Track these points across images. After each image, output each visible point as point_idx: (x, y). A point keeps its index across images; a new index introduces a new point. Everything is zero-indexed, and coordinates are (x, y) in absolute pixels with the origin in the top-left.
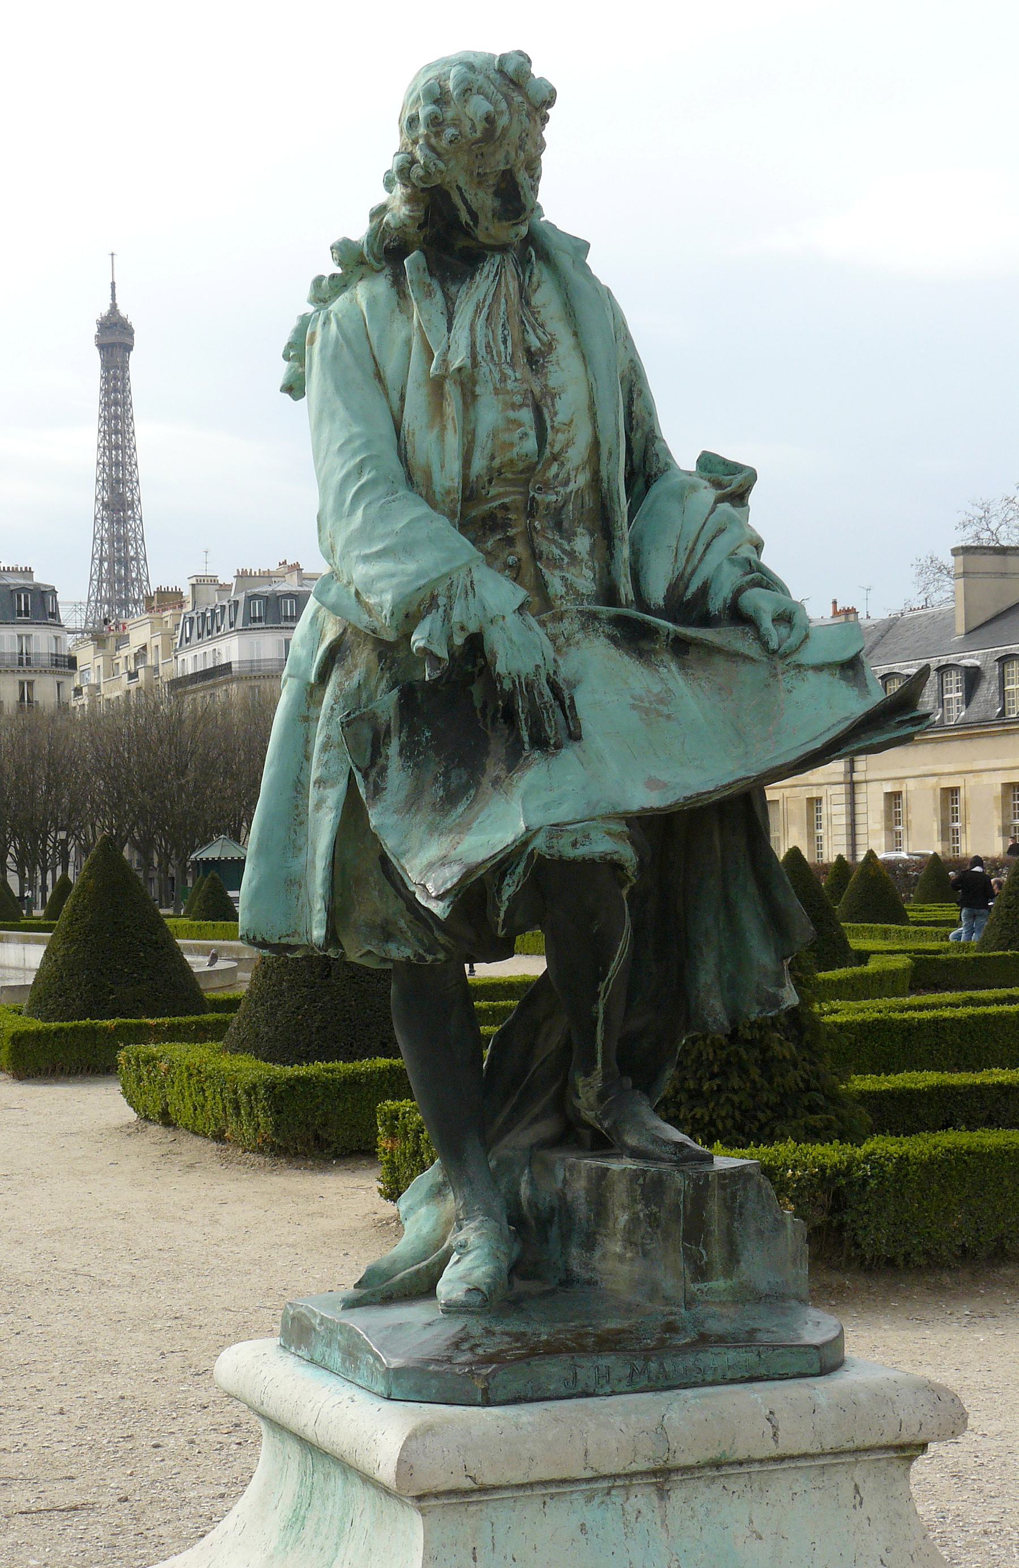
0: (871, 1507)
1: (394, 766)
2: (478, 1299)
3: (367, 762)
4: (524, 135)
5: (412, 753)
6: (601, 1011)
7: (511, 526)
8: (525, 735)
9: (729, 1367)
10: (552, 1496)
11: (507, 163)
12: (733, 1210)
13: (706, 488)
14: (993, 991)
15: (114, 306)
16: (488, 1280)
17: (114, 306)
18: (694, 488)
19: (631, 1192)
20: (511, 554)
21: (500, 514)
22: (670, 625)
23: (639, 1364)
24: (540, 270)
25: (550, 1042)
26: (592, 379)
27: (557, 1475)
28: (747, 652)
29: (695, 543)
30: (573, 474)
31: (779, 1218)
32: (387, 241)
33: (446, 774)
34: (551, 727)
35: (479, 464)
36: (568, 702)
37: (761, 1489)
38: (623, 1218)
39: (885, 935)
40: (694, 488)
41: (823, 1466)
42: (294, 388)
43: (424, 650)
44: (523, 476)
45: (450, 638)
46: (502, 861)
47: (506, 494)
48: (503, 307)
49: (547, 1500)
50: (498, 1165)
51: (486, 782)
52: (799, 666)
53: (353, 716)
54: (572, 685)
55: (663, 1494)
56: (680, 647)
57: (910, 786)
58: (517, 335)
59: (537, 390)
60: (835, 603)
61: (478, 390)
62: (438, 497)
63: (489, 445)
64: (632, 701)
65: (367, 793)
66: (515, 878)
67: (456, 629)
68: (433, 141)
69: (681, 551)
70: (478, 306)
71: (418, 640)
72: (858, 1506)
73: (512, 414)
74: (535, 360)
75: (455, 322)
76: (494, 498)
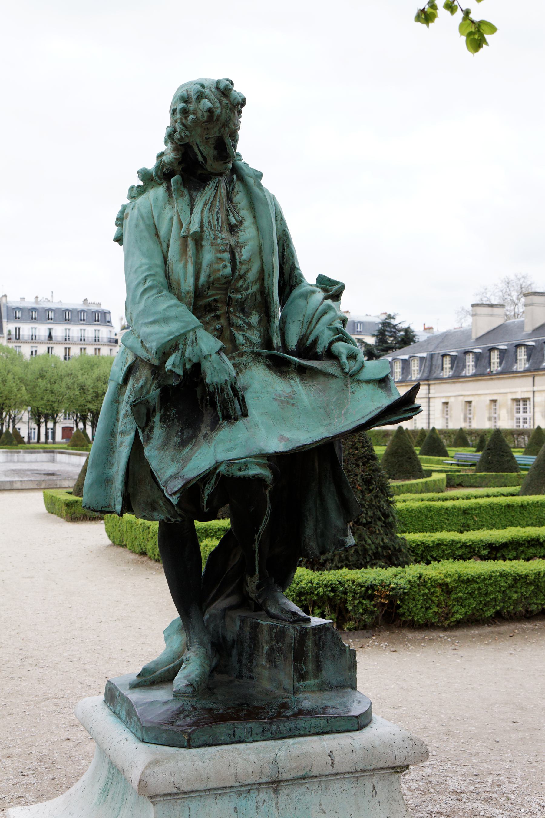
0: (381, 796)
1: (157, 426)
2: (190, 690)
3: (143, 424)
4: (228, 119)
5: (166, 421)
6: (257, 548)
7: (218, 310)
8: (220, 413)
9: (312, 727)
10: (220, 794)
11: (220, 133)
12: (319, 645)
13: (319, 292)
14: (452, 533)
16: (198, 679)
18: (313, 292)
19: (270, 635)
20: (218, 324)
21: (213, 304)
22: (296, 359)
23: (267, 726)
24: (239, 186)
25: (235, 560)
26: (261, 239)
27: (221, 785)
28: (334, 373)
29: (312, 319)
30: (250, 285)
31: (343, 648)
32: (165, 170)
33: (182, 431)
34: (232, 410)
35: (203, 279)
36: (241, 398)
37: (326, 788)
38: (266, 648)
39: (438, 463)
40: (313, 292)
41: (357, 777)
42: (119, 240)
43: (171, 371)
44: (225, 286)
45: (184, 365)
46: (204, 478)
47: (216, 294)
48: (218, 203)
49: (218, 796)
50: (210, 617)
51: (200, 435)
52: (359, 381)
53: (137, 402)
54: (245, 389)
55: (276, 791)
56: (302, 371)
57: (451, 400)
58: (224, 217)
59: (233, 244)
60: (424, 324)
61: (204, 243)
62: (183, 295)
63: (208, 270)
65: (143, 439)
66: (211, 485)
67: (187, 361)
68: (184, 121)
69: (305, 323)
70: (205, 202)
71: (168, 365)
72: (374, 796)
73: (219, 255)
74: (233, 229)
75: (194, 210)
76: (210, 297)
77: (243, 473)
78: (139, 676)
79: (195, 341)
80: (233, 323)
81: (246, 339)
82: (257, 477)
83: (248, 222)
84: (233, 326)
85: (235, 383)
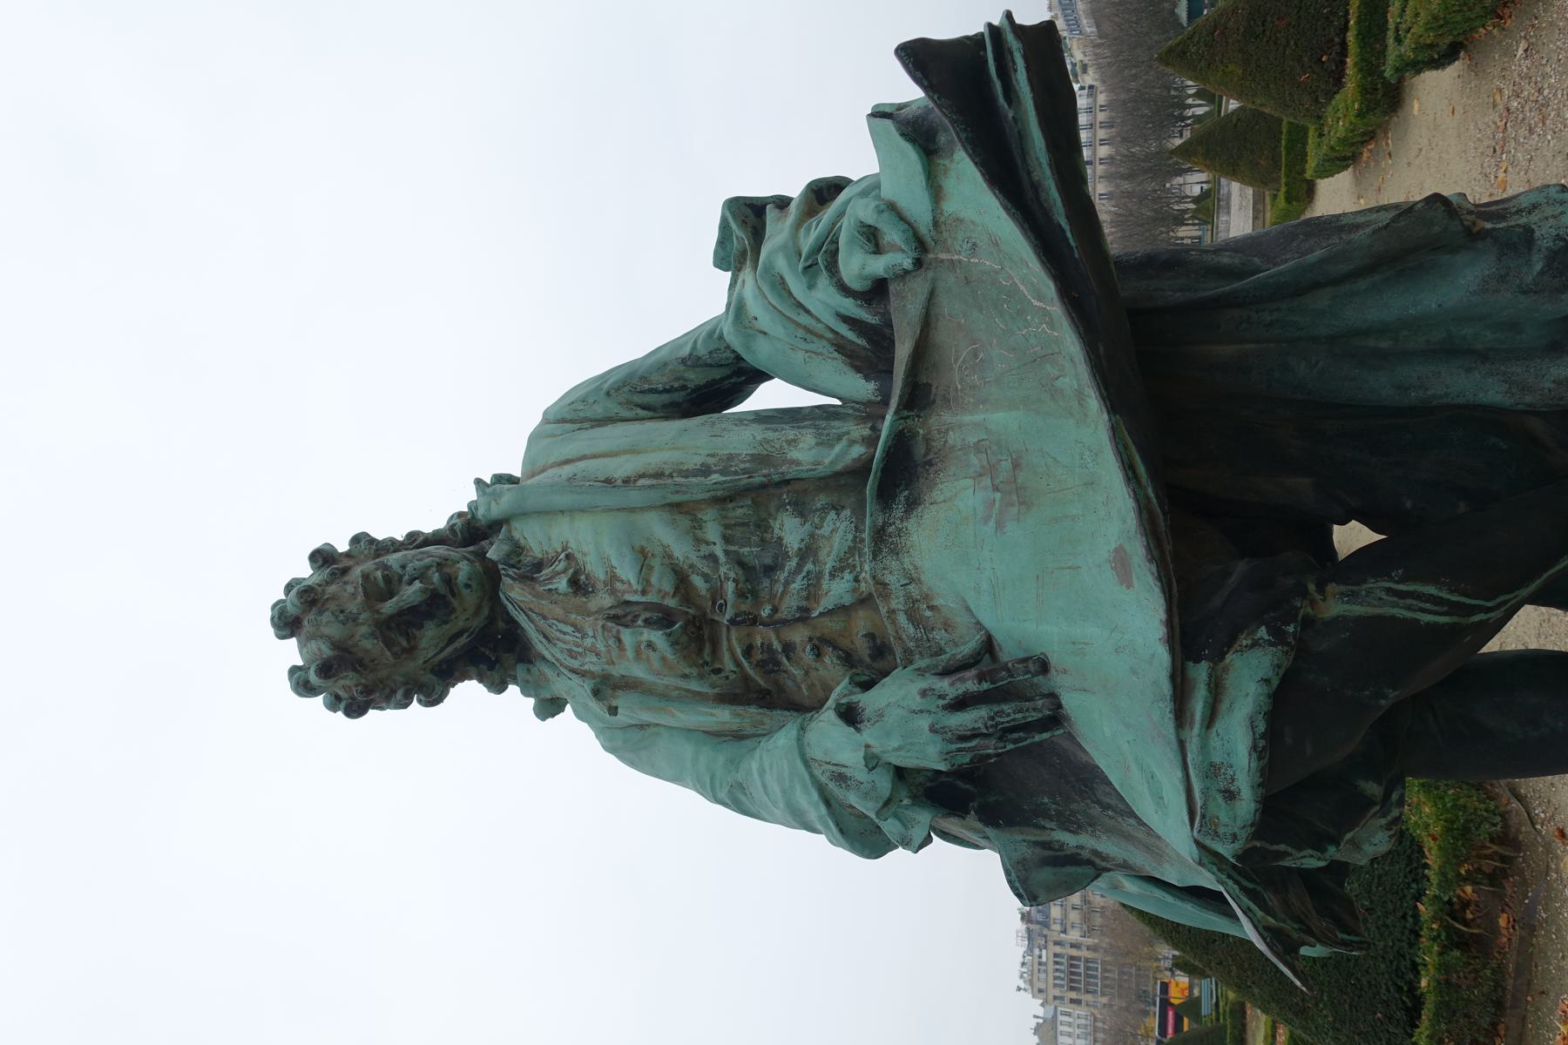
3: (1089, 870)
4: (341, 617)
7: (770, 645)
29: (798, 325)
47: (731, 650)
52: (936, 224)
64: (992, 523)
69: (808, 347)
76: (738, 664)
77: (1245, 784)
80: (800, 609)
81: (842, 569)
82: (1262, 743)
84: (807, 610)
85: (941, 697)
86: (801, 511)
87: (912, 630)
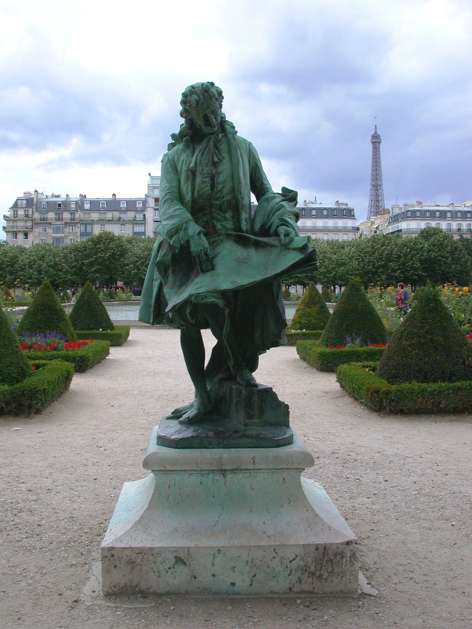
15: (376, 132)
17: (376, 132)
22: (253, 237)
23: (221, 441)
58: (210, 158)
73: (204, 180)
74: (215, 165)
78: (172, 413)
79: (186, 229)
83: (226, 161)
86: (233, 217)
87: (211, 241)
